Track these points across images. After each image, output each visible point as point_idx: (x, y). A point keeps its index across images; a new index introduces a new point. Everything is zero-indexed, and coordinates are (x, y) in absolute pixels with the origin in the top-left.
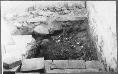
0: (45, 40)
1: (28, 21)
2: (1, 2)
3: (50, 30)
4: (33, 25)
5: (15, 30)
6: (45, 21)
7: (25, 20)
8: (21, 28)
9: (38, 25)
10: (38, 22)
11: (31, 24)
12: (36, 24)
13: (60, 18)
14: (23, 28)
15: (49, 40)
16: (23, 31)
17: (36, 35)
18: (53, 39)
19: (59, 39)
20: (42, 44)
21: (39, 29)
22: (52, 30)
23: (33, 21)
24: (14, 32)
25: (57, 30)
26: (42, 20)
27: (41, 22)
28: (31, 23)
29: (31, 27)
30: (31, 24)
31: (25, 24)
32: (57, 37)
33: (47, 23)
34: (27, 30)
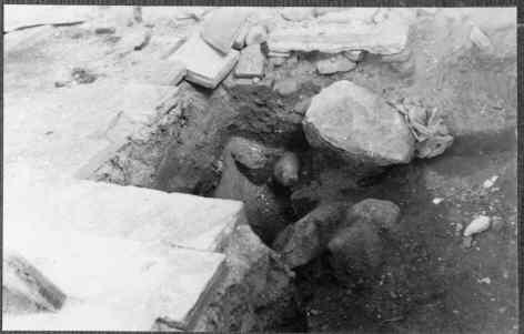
0: (366, 209)
1: (276, 41)
2: (6, 6)
3: (421, 128)
4: (303, 71)
5: (160, 116)
6: (394, 51)
7: (258, 30)
8: (226, 89)
9: (340, 75)
10: (343, 53)
11: (295, 60)
12: (325, 66)
13: (380, 209)
14: (233, 89)
15: (404, 211)
16: (233, 110)
17: (318, 149)
18: (436, 201)
19: (481, 205)
20: (337, 241)
21: (343, 111)
22: (433, 128)
23: (306, 39)
24: (154, 129)
25: (477, 129)
26: (371, 45)
27: (365, 53)
28: (292, 52)
29: (287, 86)
30: (296, 65)
31: (252, 63)
32: (464, 183)
33: (407, 66)
34: (260, 106)
